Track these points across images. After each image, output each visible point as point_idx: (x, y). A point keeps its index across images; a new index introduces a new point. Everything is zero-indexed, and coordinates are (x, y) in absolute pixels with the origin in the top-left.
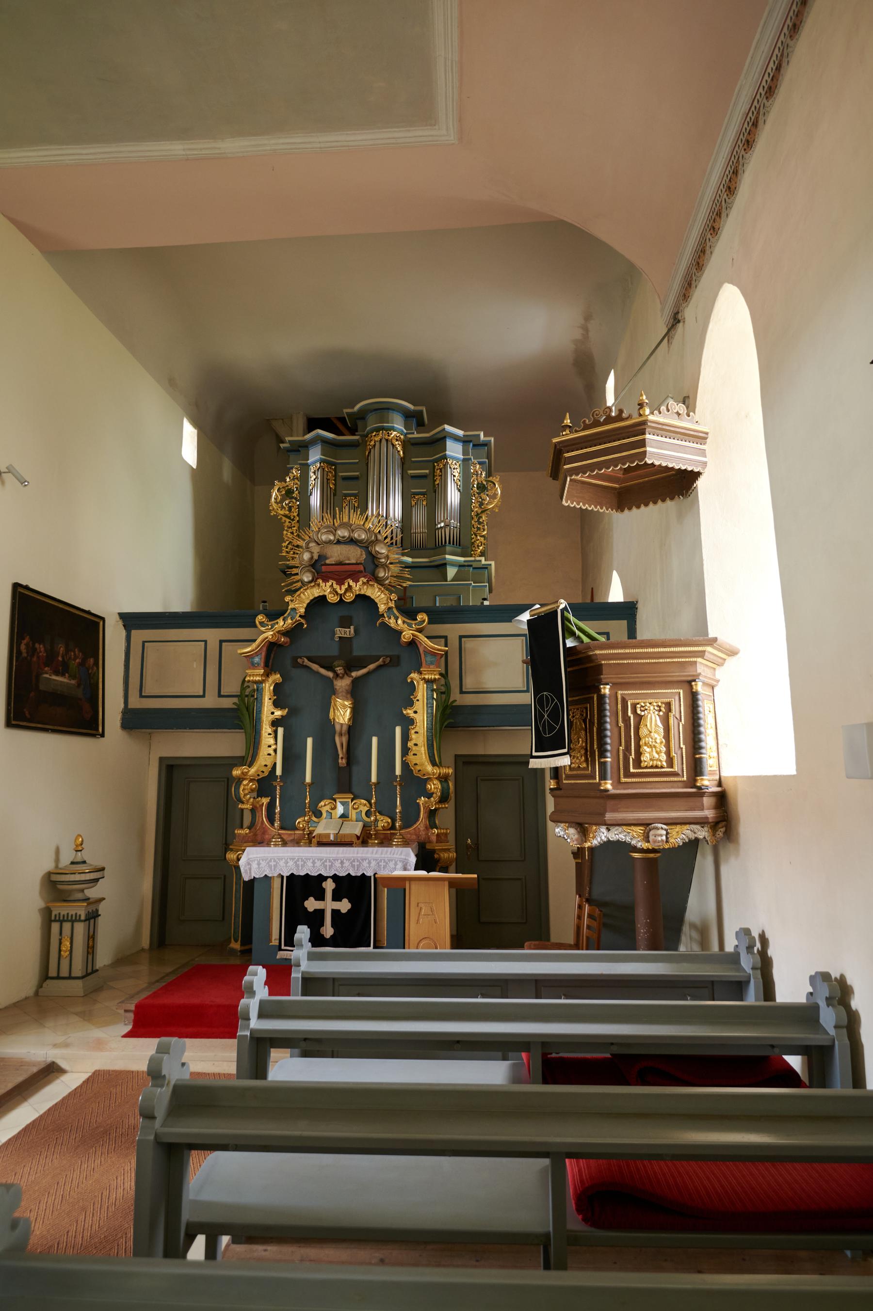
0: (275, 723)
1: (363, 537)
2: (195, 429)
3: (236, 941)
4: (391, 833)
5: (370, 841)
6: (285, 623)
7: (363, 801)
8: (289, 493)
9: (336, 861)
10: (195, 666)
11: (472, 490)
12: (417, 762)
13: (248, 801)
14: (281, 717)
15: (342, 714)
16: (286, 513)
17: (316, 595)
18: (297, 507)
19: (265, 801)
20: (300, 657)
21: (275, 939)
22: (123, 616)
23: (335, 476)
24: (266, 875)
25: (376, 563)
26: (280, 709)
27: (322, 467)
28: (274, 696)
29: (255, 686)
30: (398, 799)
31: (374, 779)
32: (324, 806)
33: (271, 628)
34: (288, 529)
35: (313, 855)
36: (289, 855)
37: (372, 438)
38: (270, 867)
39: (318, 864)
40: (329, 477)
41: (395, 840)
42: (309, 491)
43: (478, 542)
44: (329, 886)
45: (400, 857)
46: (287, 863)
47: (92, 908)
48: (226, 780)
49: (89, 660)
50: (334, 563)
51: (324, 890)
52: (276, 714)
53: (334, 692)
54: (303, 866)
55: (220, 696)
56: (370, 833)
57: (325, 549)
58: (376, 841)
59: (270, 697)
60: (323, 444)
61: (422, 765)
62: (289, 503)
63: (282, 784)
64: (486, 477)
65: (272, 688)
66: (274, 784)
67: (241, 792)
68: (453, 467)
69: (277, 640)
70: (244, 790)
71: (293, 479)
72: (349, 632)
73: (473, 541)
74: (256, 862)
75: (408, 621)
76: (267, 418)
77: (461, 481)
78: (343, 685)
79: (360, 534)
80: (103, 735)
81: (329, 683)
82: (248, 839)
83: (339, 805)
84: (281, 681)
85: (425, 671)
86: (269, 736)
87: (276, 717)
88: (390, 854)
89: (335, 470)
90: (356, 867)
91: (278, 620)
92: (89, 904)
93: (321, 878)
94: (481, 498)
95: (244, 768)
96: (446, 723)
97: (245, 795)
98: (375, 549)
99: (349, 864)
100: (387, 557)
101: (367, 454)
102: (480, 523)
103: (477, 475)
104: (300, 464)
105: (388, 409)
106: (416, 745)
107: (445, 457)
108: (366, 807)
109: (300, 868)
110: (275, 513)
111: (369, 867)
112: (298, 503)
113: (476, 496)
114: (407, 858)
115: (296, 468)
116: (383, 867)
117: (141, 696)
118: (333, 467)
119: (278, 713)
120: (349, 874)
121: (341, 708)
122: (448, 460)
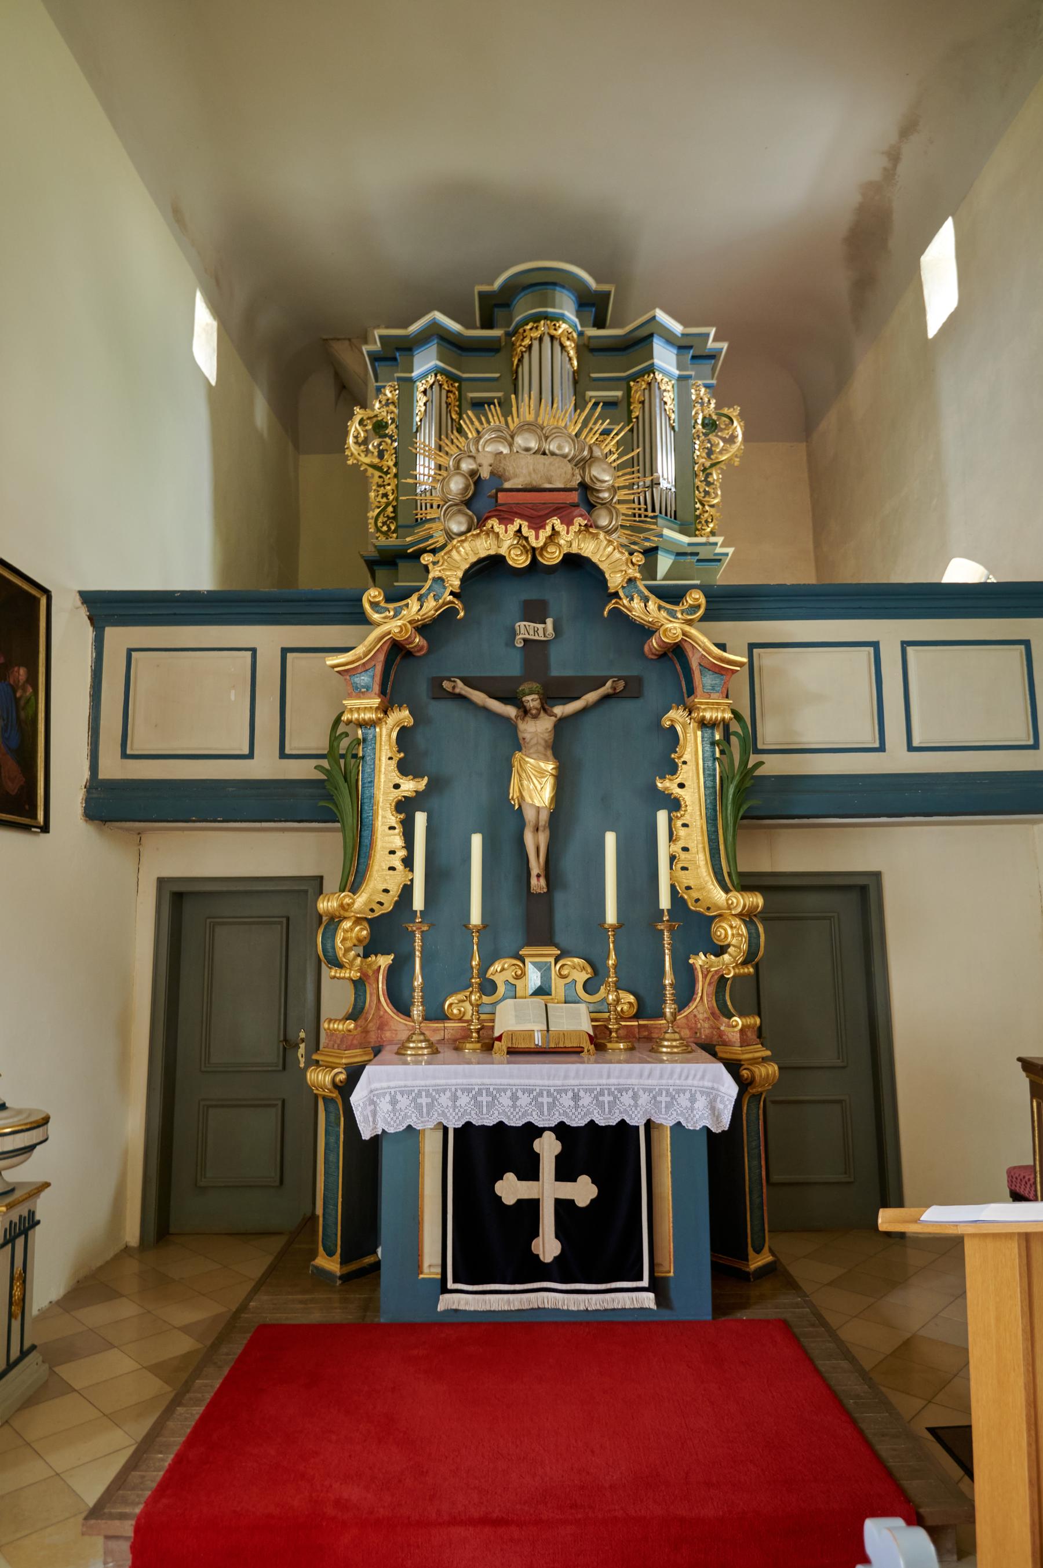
0: (405, 807)
1: (567, 450)
2: (215, 319)
3: (330, 1253)
4: (639, 1025)
5: (609, 1045)
6: (422, 606)
7: (576, 960)
8: (379, 427)
9: (563, 1095)
10: (233, 698)
11: (695, 428)
12: (692, 884)
13: (352, 963)
14: (414, 794)
15: (539, 788)
16: (374, 460)
17: (483, 554)
18: (393, 451)
19: (384, 961)
20: (449, 679)
21: (430, 1266)
22: (89, 599)
23: (460, 399)
24: (409, 1127)
25: (592, 499)
26: (411, 777)
27: (438, 381)
28: (399, 752)
29: (360, 732)
30: (667, 958)
31: (611, 917)
32: (501, 971)
33: (395, 616)
34: (379, 489)
35: (512, 1082)
36: (460, 1081)
37: (525, 334)
38: (419, 1107)
39: (524, 1100)
40: (449, 400)
41: (666, 1043)
42: (415, 424)
43: (706, 515)
44: (548, 1148)
45: (701, 1083)
46: (455, 1098)
47: (23, 1210)
48: (284, 920)
49: (16, 669)
50: (520, 487)
51: (536, 1157)
52: (403, 787)
53: (517, 744)
54: (490, 1105)
55: (283, 755)
56: (606, 1027)
57: (503, 461)
58: (621, 1046)
59: (390, 755)
60: (441, 342)
61: (702, 888)
62: (380, 444)
63: (425, 928)
64: (715, 408)
65: (394, 735)
66: (410, 929)
67: (340, 945)
68: (663, 387)
69: (406, 639)
70: (344, 940)
71: (387, 404)
72: (543, 630)
73: (698, 513)
74: (388, 1098)
75: (668, 606)
76: (325, 337)
77: (676, 412)
78: (539, 730)
79: (562, 444)
80: (45, 829)
81: (509, 727)
82: (352, 1040)
83: (530, 969)
84: (412, 723)
85: (701, 703)
86: (392, 831)
87: (406, 794)
88: (680, 1078)
89: (459, 389)
90: (606, 1106)
91: (409, 601)
92: (10, 1207)
93: (532, 1131)
94: (709, 442)
95: (345, 897)
96: (745, 807)
97: (347, 950)
98: (590, 473)
99: (590, 1099)
100: (614, 490)
101: (516, 362)
102: (709, 484)
103: (702, 404)
104: (399, 379)
105: (554, 284)
106: (685, 849)
107: (651, 370)
108: (584, 972)
109: (485, 1109)
110: (355, 462)
111: (636, 1106)
112: (396, 444)
113: (701, 439)
114: (716, 1086)
115: (391, 386)
116: (666, 1107)
117: (125, 755)
118: (457, 385)
119: (410, 786)
120: (592, 1122)
121: (534, 775)
122: (656, 373)
